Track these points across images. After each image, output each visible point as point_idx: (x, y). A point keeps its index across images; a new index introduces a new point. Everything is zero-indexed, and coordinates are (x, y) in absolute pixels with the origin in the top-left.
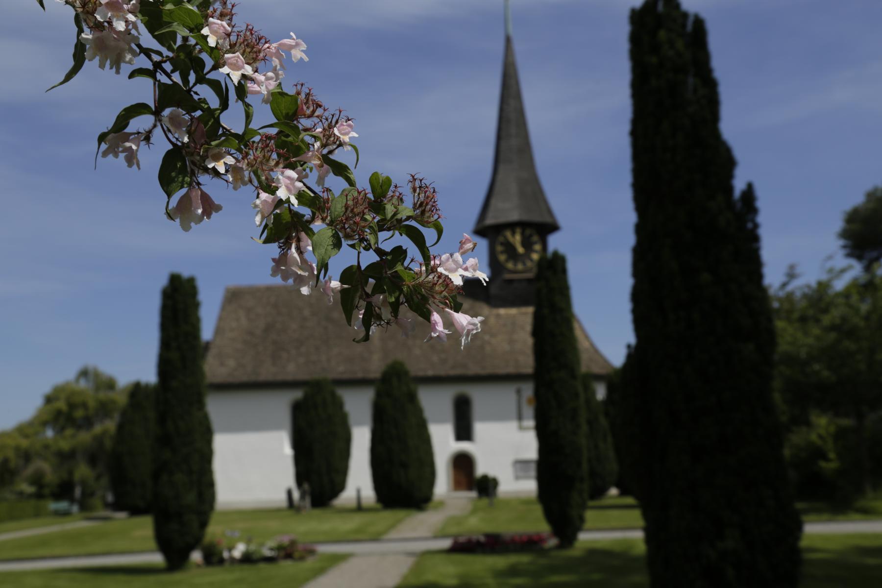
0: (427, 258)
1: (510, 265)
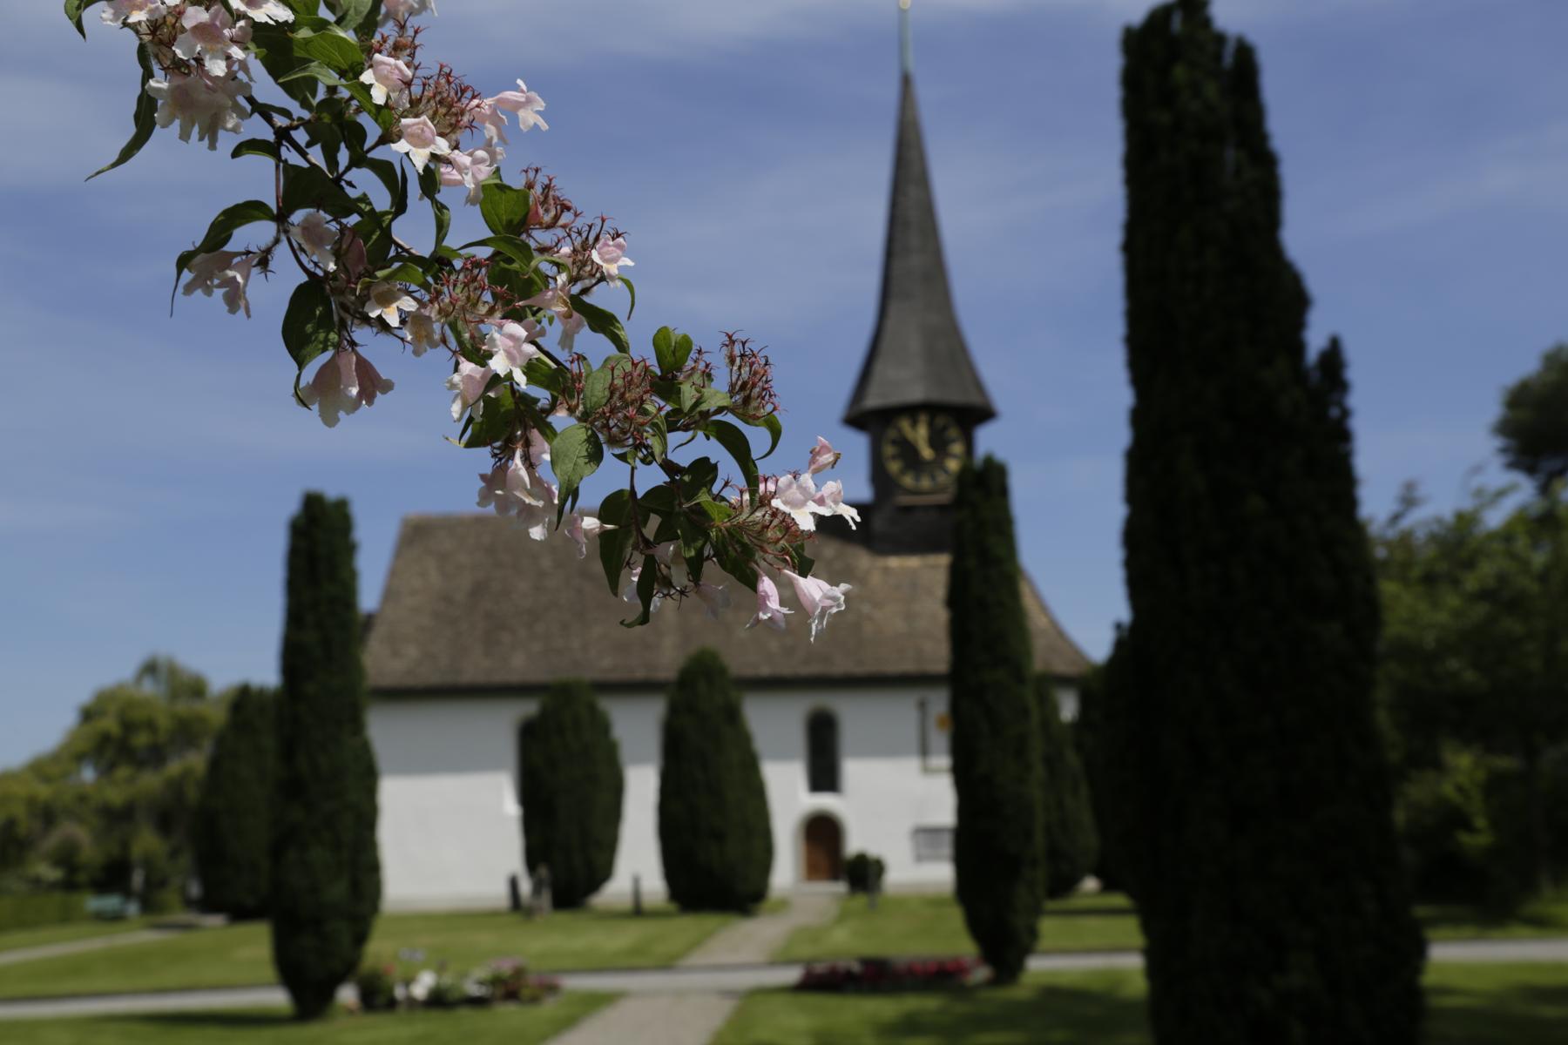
0: (752, 479)
1: (908, 480)
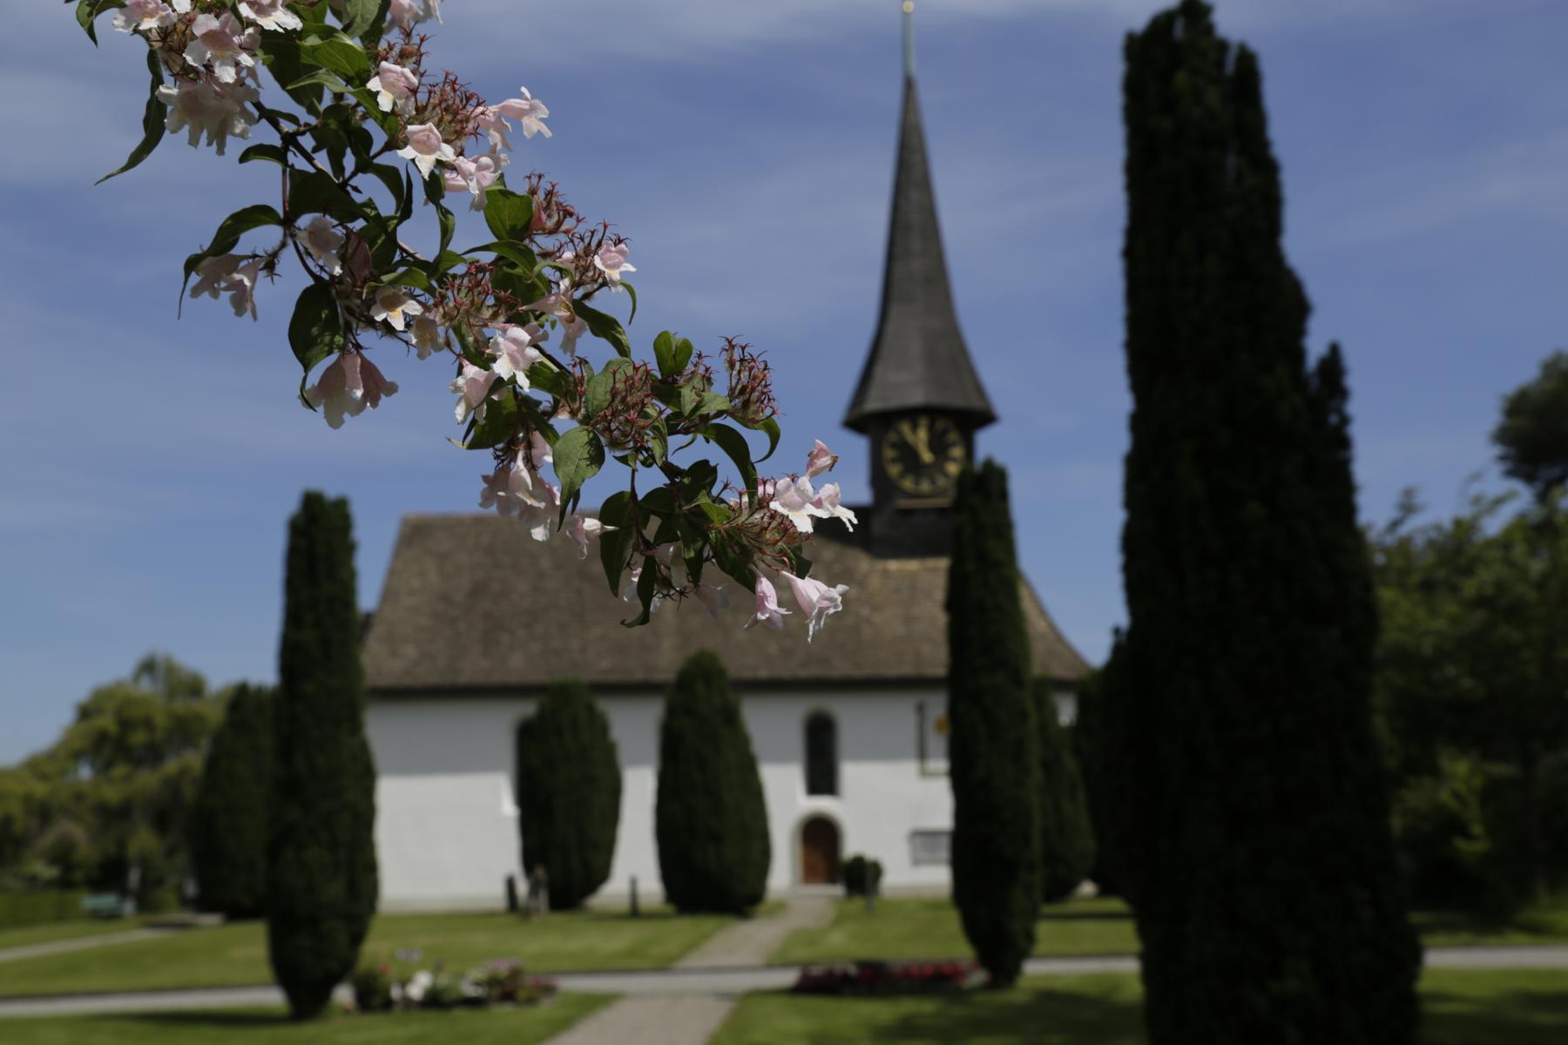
0: (751, 482)
1: (908, 484)
